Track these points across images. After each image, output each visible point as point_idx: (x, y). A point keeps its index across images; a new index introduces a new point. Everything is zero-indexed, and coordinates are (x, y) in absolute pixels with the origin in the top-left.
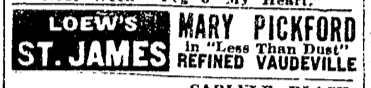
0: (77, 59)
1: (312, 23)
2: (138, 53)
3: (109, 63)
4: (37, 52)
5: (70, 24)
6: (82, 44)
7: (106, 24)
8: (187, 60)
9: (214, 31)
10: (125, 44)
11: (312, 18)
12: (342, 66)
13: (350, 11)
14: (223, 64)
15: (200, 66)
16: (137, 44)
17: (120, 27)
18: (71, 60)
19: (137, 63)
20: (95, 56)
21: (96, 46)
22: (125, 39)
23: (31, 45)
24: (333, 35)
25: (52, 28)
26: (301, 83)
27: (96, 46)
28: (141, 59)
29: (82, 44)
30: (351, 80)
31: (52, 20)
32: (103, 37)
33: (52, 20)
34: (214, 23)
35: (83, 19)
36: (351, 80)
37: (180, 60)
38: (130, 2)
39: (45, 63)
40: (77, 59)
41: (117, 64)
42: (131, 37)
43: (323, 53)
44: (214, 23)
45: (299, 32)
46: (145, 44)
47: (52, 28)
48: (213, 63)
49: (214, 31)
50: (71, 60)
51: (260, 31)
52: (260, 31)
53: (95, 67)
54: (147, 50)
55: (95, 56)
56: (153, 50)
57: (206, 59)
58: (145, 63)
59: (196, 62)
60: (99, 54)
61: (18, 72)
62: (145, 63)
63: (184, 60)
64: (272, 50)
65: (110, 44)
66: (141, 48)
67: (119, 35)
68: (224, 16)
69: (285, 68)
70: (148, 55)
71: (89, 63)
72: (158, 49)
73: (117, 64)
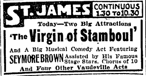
0: (41, 12)
2: (75, 10)
3: (59, 14)
12: (16, 62)
13: (66, 51)
15: (19, 62)
16: (75, 6)
19: (75, 13)
20: (52, 10)
21: (52, 7)
22: (31, 7)
40: (41, 12)
43: (134, 58)
48: (114, 7)
50: (38, 13)
53: (52, 16)
55: (52, 10)
58: (79, 14)
62: (79, 14)
64: (65, 68)
66: (77, 8)
69: (123, 25)
71: (49, 14)
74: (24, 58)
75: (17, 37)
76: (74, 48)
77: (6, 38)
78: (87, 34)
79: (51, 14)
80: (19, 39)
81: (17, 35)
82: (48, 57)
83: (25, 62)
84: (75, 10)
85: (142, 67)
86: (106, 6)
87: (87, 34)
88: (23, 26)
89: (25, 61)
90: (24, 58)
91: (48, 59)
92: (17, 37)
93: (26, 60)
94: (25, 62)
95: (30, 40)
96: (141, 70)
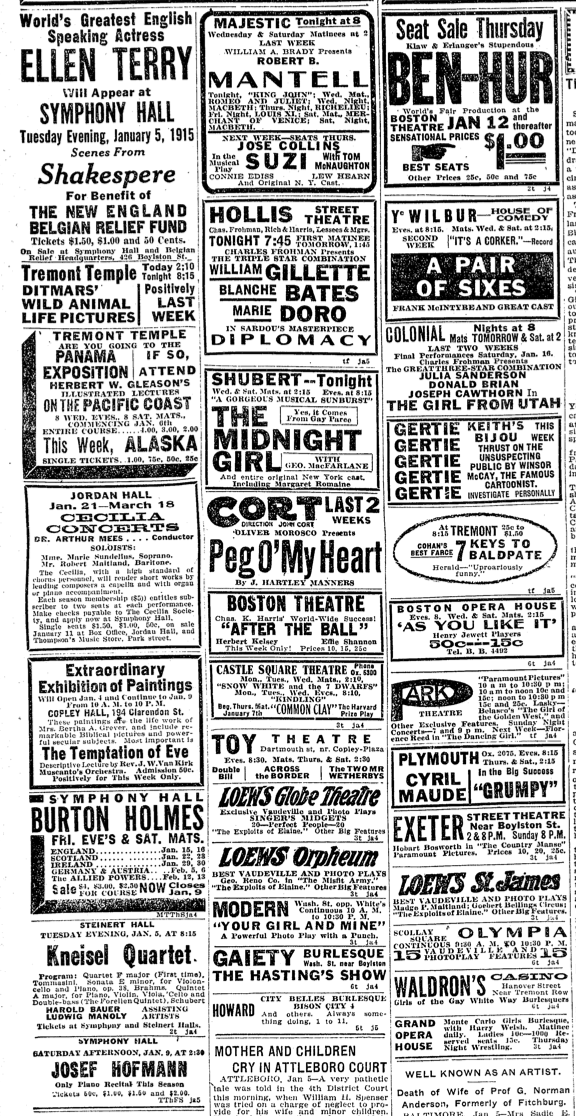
10: (503, 270)
12: (44, 75)
16: (502, 282)
19: (502, 293)
24: (534, 90)
35: (437, 283)
37: (98, 228)
38: (421, 1111)
44: (168, 58)
45: (307, 558)
49: (168, 67)
51: (216, 560)
52: (216, 560)
54: (510, 286)
56: (515, 286)
57: (157, 225)
59: (136, 228)
62: (509, 294)
66: (441, 285)
68: (413, 840)
70: (511, 289)
71: (485, 294)
75: (395, 405)
92: (395, 405)
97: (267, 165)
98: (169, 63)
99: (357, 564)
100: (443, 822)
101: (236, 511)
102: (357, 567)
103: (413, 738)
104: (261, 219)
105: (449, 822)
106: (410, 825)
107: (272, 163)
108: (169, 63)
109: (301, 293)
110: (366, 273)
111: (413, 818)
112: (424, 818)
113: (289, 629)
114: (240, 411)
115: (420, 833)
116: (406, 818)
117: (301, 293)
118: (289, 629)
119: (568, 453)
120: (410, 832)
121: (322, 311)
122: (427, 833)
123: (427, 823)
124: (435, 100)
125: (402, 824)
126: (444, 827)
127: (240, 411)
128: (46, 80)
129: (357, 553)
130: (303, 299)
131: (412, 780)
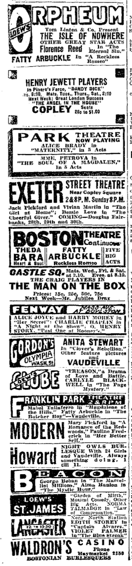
0: (32, 511)
1: (107, 183)
3: (43, 512)
4: (20, 509)
5: (32, 500)
6: (34, 506)
7: (42, 499)
8: (44, 58)
9: (58, 195)
10: (49, 506)
11: (107, 181)
14: (79, 186)
16: (53, 506)
17: (46, 500)
18: (30, 511)
19: (52, 512)
21: (39, 507)
23: (18, 507)
25: (25, 501)
26: (131, 318)
27: (39, 507)
28: (54, 510)
29: (34, 506)
30: (129, 559)
31: (25, 498)
32: (41, 504)
33: (25, 498)
34: (58, 188)
35: (35, 498)
36: (129, 559)
39: (23, 512)
40: (32, 511)
41: (46, 512)
42: (51, 503)
44: (58, 188)
46: (55, 505)
47: (25, 501)
49: (58, 195)
50: (30, 511)
56: (58, 507)
58: (55, 512)
60: (40, 509)
61: (9, 501)
62: (55, 512)
63: (43, 58)
65: (44, 506)
67: (46, 503)
70: (57, 509)
71: (37, 512)
72: (60, 507)
73: (46, 512)
74: (16, 428)
75: (15, 286)
76: (28, 8)
77: (9, 198)
78: (103, 82)
79: (39, 513)
80: (17, 288)
81: (14, 283)
82: (46, 545)
83: (17, 437)
84: (53, 509)
85: (124, 170)
86: (53, 288)
87: (103, 82)
88: (11, 367)
89: (17, 433)
90: (16, 428)
91: (45, 550)
92: (15, 286)
93: (19, 433)
94: (17, 437)
95: (17, 20)
96: (124, 128)
97: (70, 258)
98: (58, 192)
99: (40, 460)
100: (46, 188)
101: (39, 109)
102: (40, 461)
103: (44, 298)
104: (111, 364)
105: (51, 187)
106: (22, 189)
107: (71, 257)
108: (58, 192)
109: (20, 257)
110: (98, 286)
111: (24, 183)
112: (32, 183)
113: (42, 36)
114: (90, 284)
115: (30, 197)
116: (19, 183)
117: (20, 257)
118: (42, 36)
119: (129, 138)
120: (22, 195)
121: (32, 256)
122: (35, 197)
123: (35, 188)
124: (53, 201)
125: (15, 188)
126: (48, 192)
127: (90, 284)
128: (66, 60)
129: (40, 455)
130: (21, 260)
131: (48, 280)
